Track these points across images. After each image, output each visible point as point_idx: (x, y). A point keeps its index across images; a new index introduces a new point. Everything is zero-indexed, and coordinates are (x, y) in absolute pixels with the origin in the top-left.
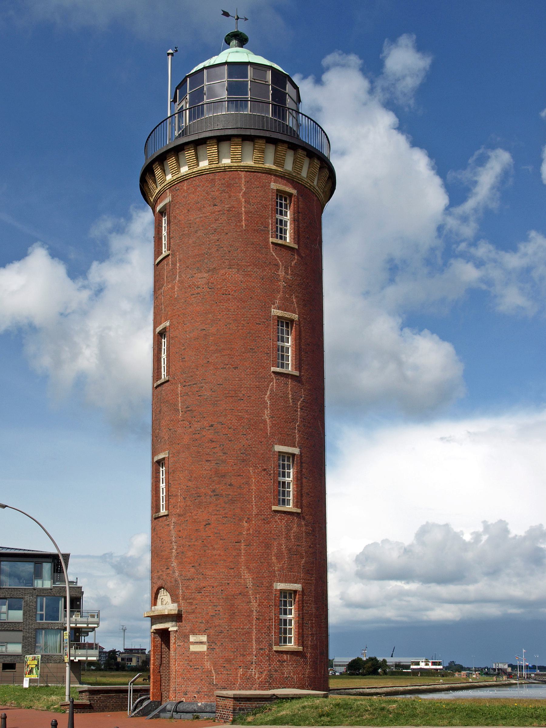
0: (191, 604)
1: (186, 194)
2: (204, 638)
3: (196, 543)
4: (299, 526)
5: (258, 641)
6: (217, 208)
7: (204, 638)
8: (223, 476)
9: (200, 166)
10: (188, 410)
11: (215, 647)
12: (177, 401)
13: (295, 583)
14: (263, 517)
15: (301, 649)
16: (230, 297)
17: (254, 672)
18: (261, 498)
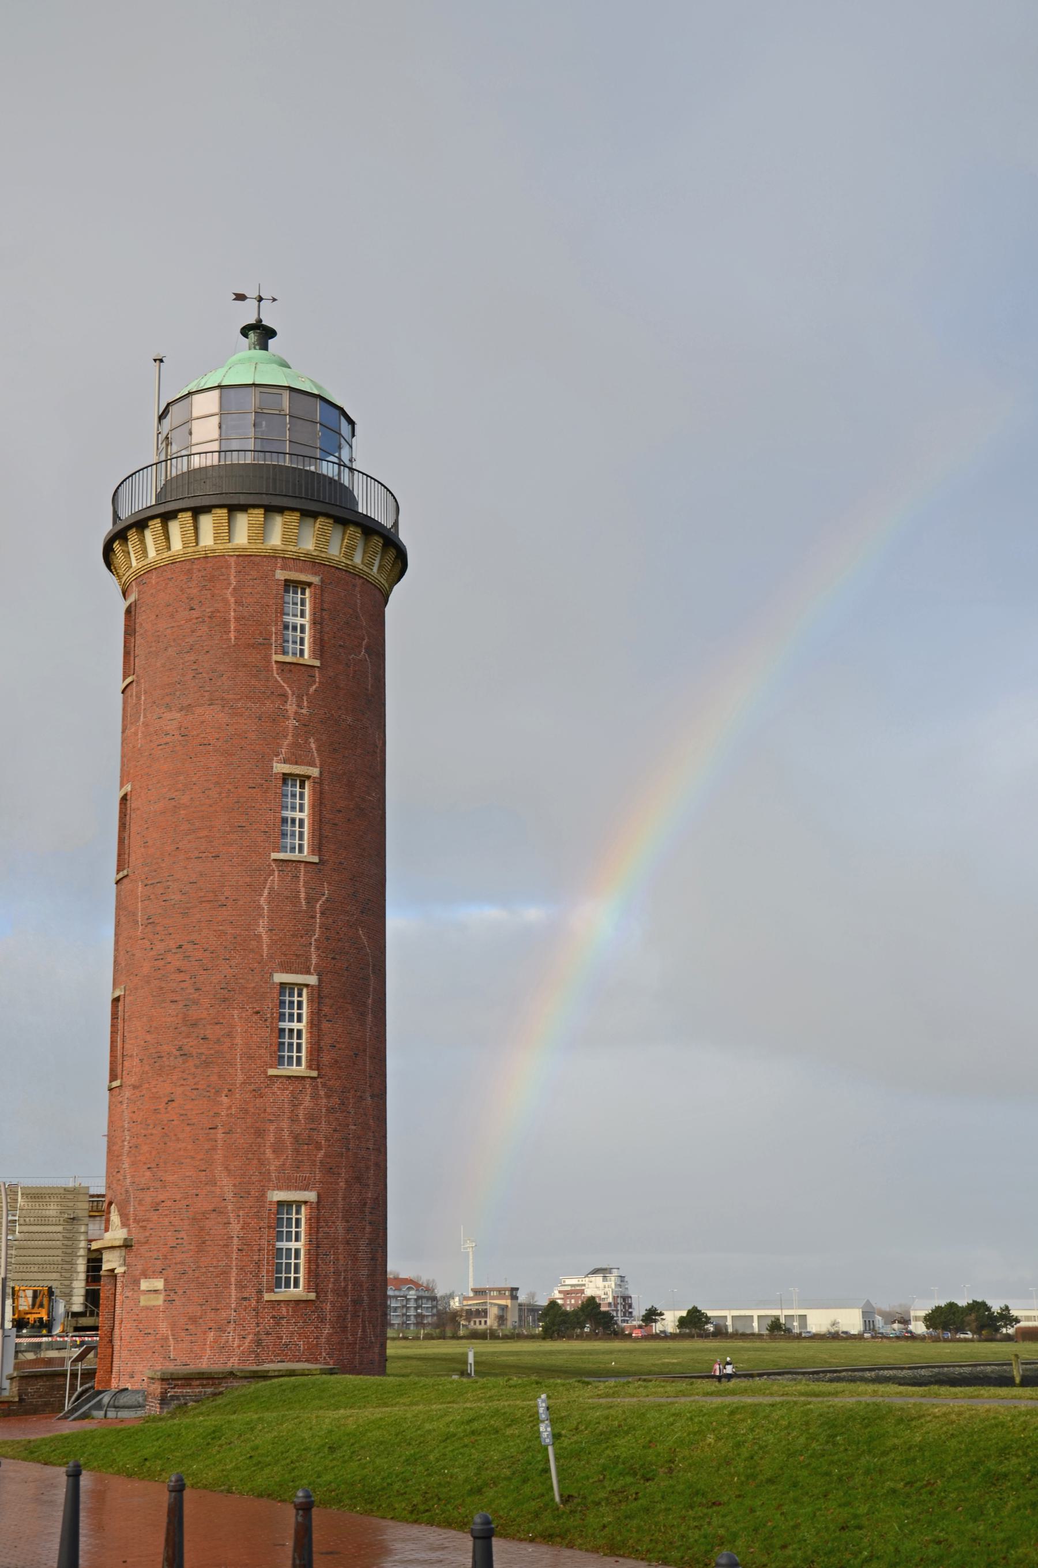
0: (144, 1228)
1: (153, 591)
2: (159, 1284)
3: (154, 1132)
4: (315, 1097)
5: (240, 1286)
6: (195, 614)
7: (159, 1284)
8: (194, 1025)
9: (173, 549)
10: (150, 922)
11: (175, 1297)
12: (137, 908)
13: (306, 1188)
14: (253, 1087)
15: (312, 1296)
16: (211, 748)
17: (231, 1336)
18: (250, 1057)
